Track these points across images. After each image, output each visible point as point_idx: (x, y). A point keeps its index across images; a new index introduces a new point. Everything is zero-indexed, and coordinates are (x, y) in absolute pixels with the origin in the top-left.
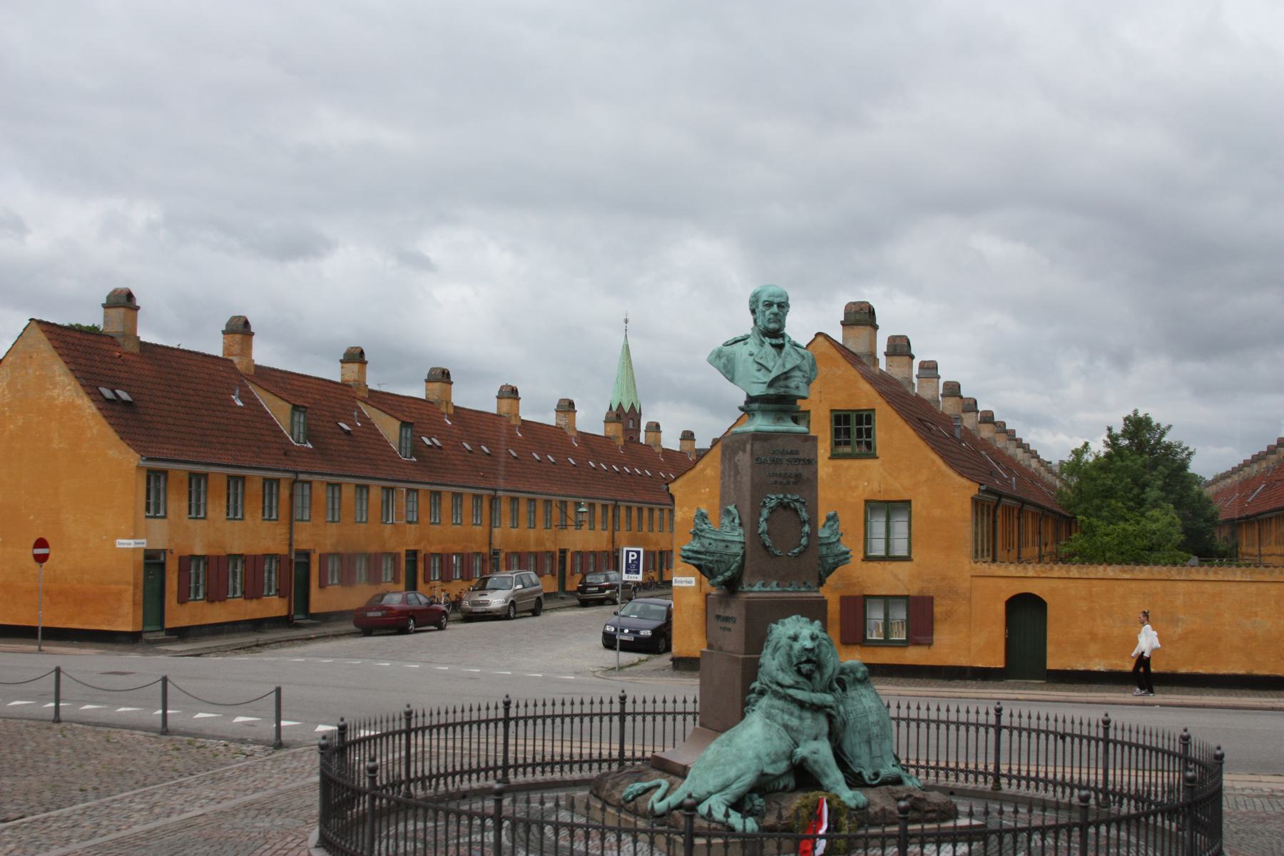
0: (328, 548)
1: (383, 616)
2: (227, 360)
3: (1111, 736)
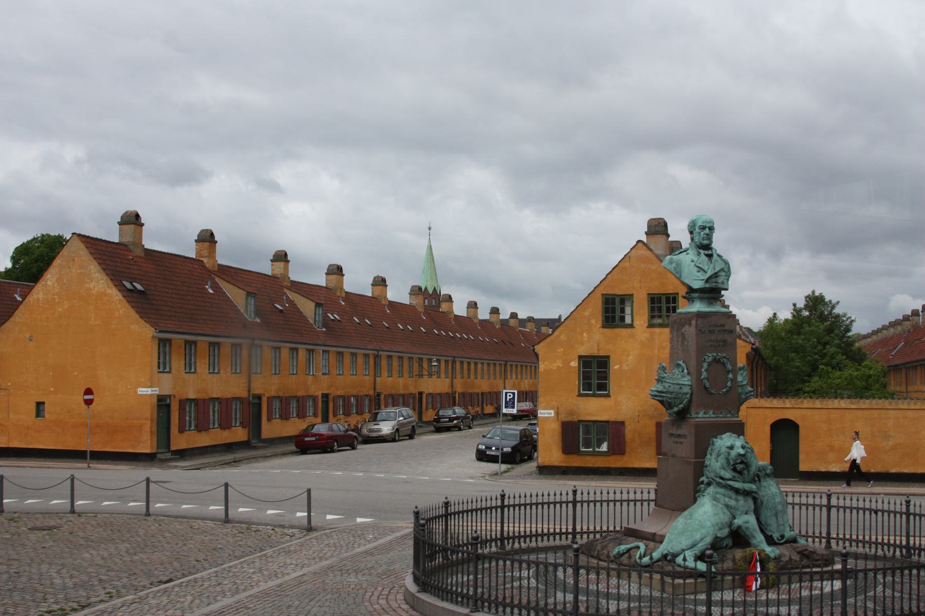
0: (273, 394)
1: (316, 440)
2: (199, 260)
3: (912, 510)
